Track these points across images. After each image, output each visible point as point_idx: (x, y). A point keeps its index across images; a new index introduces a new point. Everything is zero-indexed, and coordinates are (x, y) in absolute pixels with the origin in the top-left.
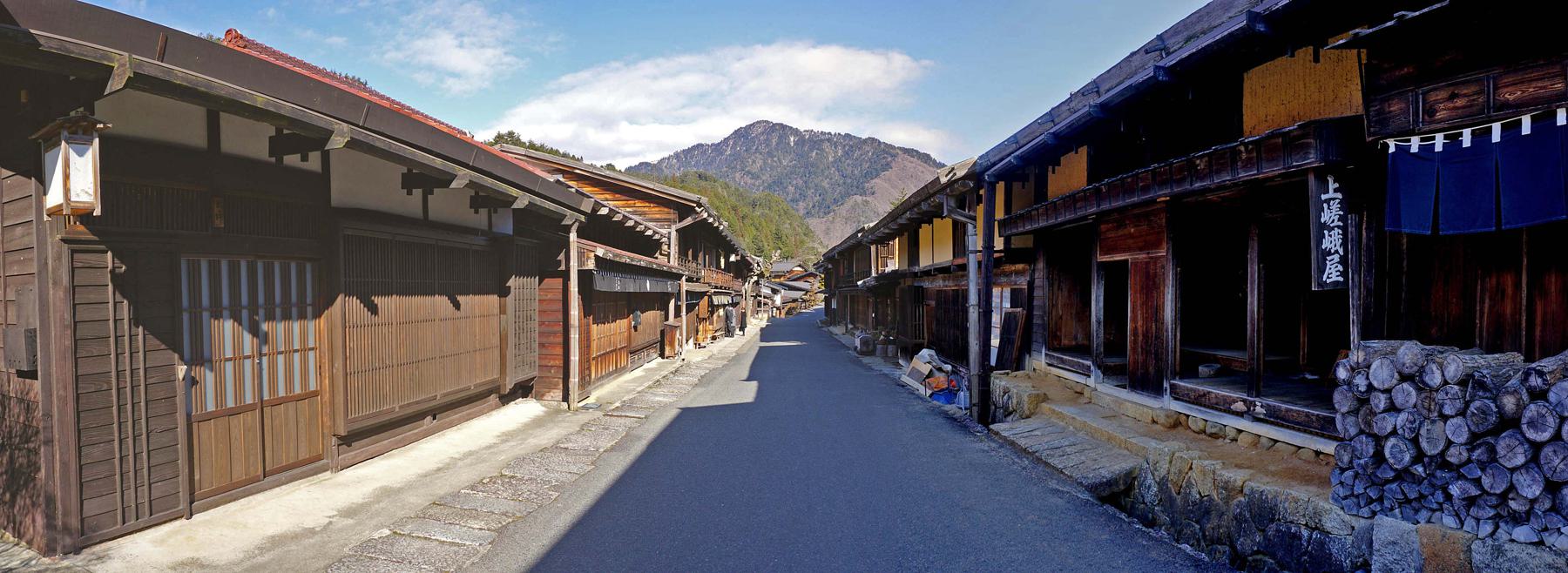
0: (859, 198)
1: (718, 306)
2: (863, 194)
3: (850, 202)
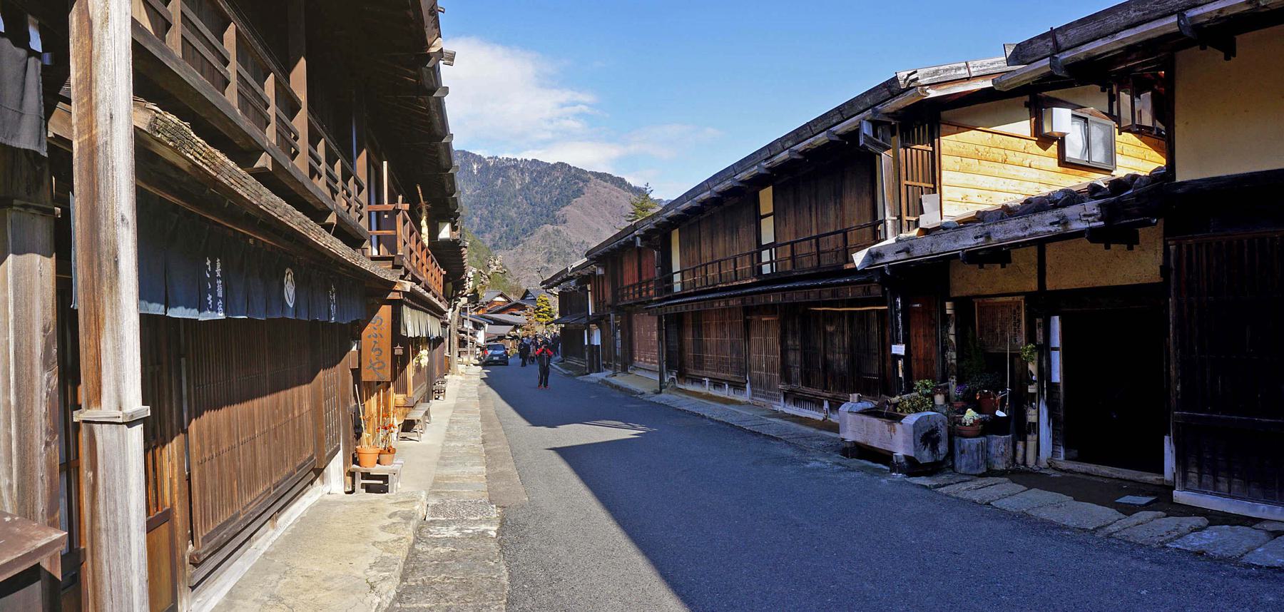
0: (549, 228)
1: (417, 343)
2: (555, 222)
3: (540, 232)
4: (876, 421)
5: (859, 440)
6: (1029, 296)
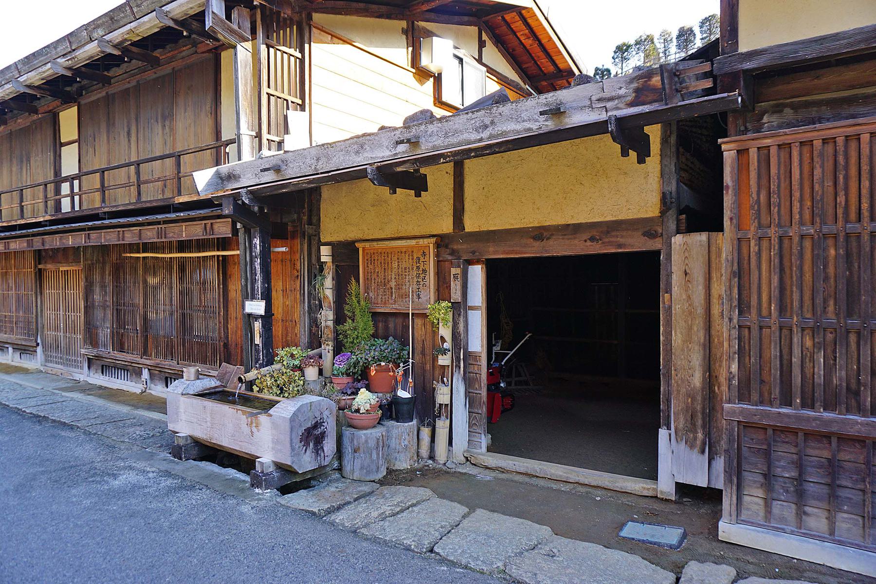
4: (226, 409)
5: (200, 434)
6: (442, 241)
